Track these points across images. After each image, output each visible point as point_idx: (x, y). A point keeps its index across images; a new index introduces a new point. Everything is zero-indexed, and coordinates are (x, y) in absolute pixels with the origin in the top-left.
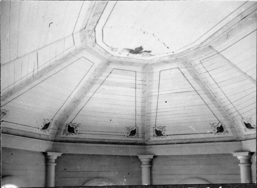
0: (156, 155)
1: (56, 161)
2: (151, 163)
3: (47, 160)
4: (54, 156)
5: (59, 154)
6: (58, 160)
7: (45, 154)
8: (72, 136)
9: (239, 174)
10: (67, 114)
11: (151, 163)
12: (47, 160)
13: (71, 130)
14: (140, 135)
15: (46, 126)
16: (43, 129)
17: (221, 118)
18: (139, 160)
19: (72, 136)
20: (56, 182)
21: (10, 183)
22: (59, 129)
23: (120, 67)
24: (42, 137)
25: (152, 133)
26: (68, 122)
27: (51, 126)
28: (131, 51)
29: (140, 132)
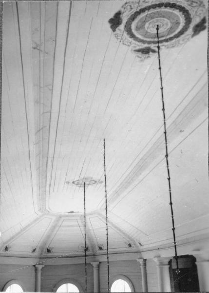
0: (101, 261)
1: (42, 270)
2: (99, 266)
3: (36, 270)
4: (40, 267)
5: (43, 266)
6: (42, 269)
7: (34, 266)
8: (49, 255)
9: (141, 272)
10: (45, 243)
11: (99, 266)
12: (36, 270)
13: (49, 251)
14: (91, 251)
15: (34, 250)
16: (33, 252)
17: (128, 240)
18: (92, 265)
19: (49, 255)
20: (61, 7)
21: (16, 283)
22: (42, 251)
23: (67, 218)
24: (32, 256)
25: (97, 248)
26: (47, 246)
27: (37, 250)
28: (69, 212)
29: (90, 248)
